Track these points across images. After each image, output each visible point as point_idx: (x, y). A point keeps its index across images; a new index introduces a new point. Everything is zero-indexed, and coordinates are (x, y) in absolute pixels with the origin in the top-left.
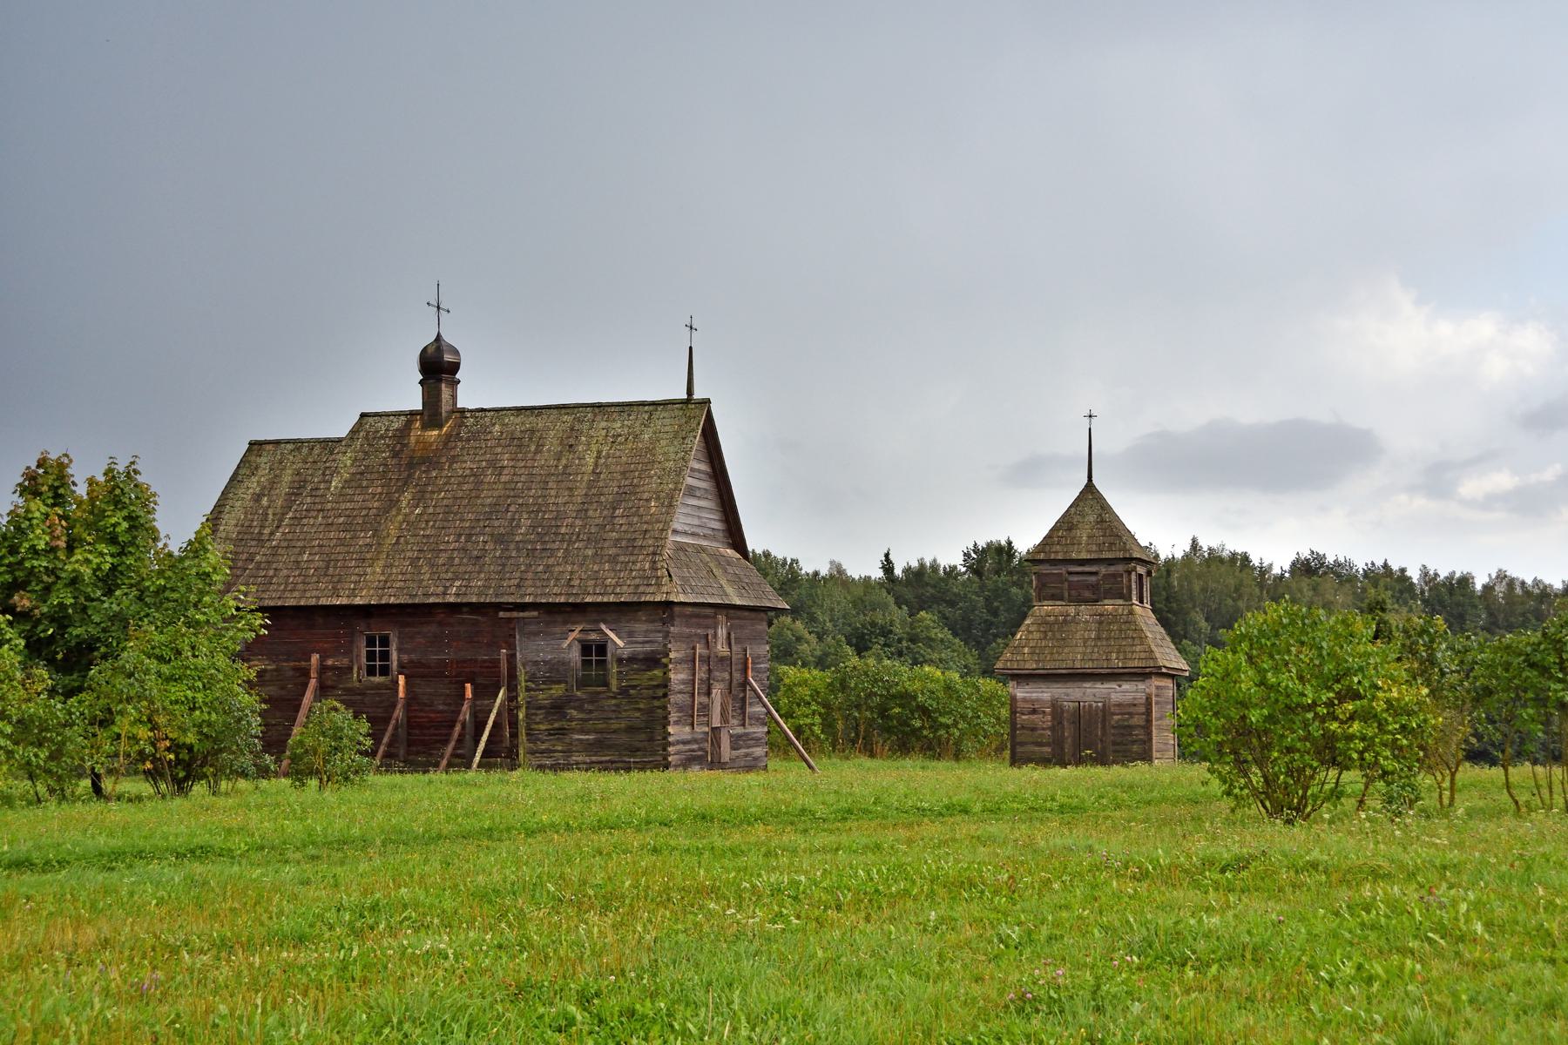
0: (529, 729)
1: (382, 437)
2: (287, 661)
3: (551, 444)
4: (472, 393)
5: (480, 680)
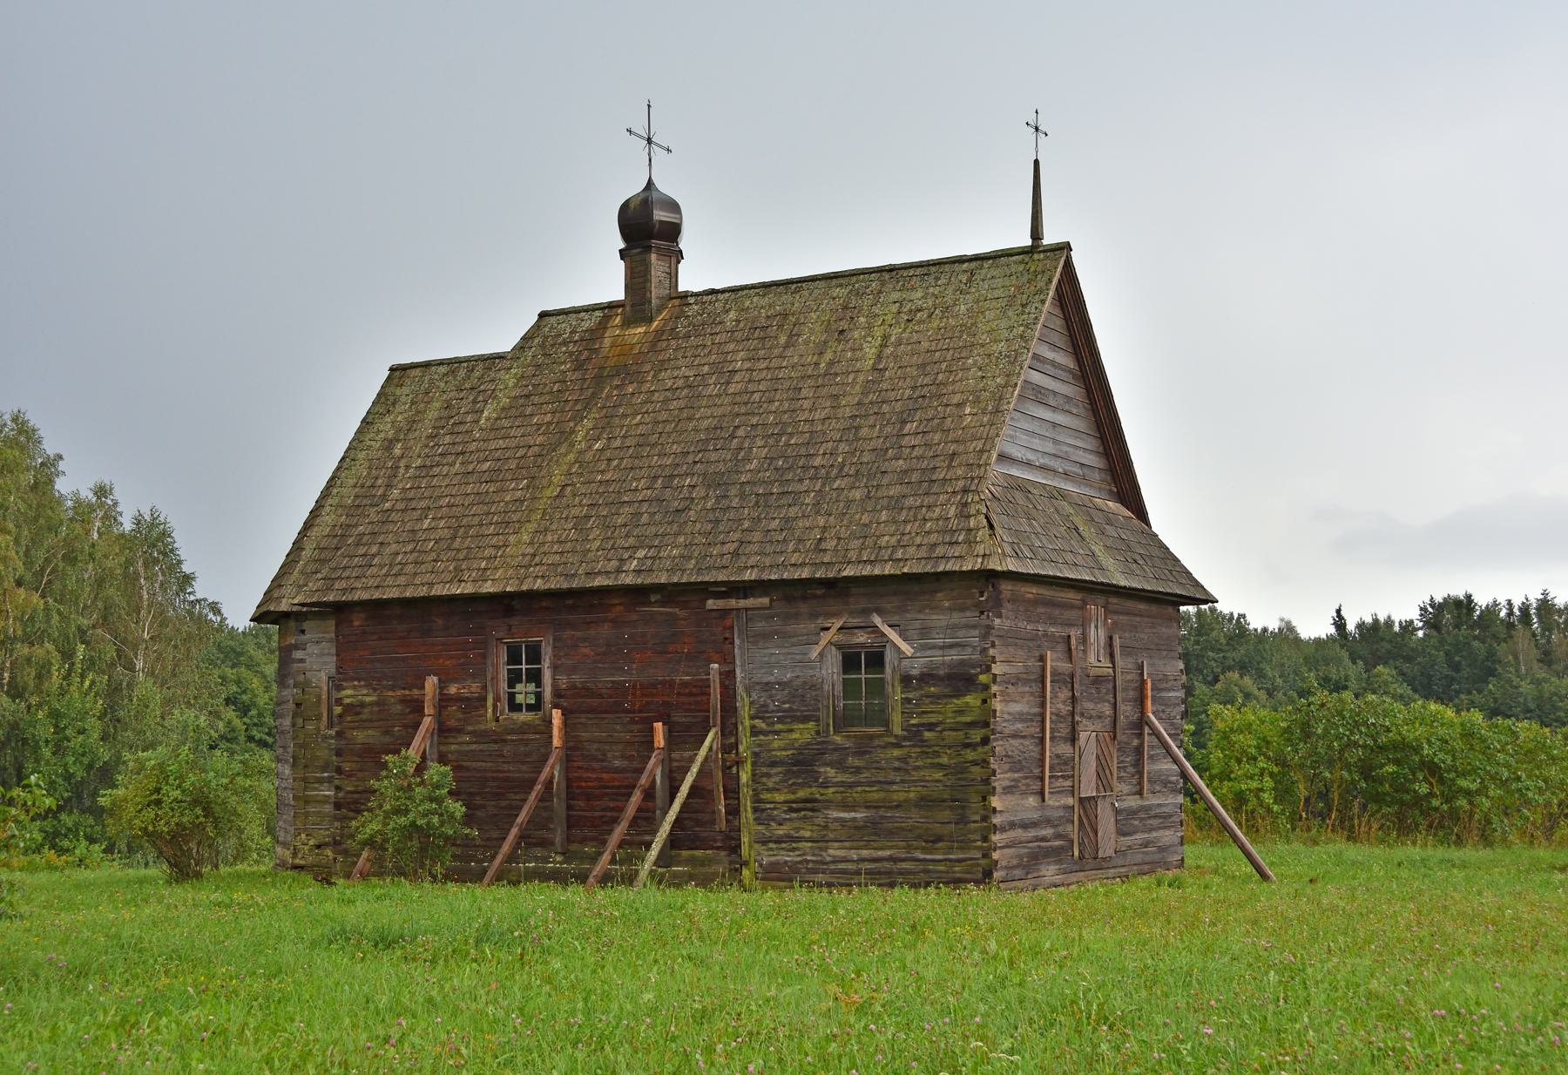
0: (757, 800)
1: (565, 343)
2: (393, 688)
3: (812, 332)
4: (699, 271)
5: (678, 717)
